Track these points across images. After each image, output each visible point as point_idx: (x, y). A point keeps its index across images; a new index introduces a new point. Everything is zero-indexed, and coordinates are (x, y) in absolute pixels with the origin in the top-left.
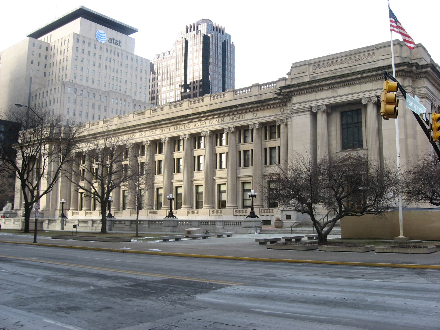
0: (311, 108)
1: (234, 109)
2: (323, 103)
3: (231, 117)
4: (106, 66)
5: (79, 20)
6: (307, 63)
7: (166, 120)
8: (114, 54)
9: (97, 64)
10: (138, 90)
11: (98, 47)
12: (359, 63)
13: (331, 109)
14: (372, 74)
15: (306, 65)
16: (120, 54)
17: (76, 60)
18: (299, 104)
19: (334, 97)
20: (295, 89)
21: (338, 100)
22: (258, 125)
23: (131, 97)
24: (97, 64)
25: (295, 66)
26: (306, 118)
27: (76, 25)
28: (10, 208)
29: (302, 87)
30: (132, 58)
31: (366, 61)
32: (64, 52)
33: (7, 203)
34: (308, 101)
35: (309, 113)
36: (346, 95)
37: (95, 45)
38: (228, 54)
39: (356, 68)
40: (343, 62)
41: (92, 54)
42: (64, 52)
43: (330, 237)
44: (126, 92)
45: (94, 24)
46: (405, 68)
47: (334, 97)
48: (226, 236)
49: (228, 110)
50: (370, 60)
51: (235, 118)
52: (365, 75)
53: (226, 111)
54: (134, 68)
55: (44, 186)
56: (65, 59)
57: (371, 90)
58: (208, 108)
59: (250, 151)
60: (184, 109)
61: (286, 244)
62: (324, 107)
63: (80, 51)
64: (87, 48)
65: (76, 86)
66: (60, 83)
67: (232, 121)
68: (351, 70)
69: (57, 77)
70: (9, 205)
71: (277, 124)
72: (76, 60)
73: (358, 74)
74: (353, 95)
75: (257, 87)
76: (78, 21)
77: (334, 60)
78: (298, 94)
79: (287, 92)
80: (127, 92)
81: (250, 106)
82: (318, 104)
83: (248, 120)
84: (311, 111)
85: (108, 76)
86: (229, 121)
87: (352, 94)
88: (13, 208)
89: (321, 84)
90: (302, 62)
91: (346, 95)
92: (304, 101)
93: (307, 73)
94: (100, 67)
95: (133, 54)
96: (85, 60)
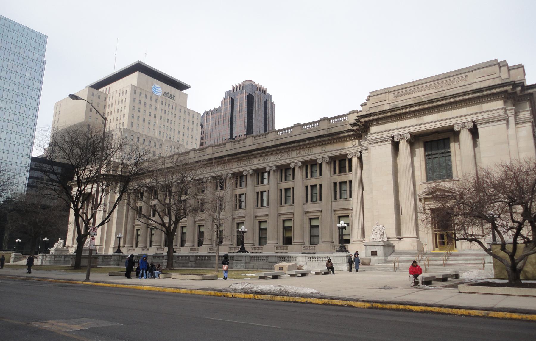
0: (393, 137)
1: (301, 143)
2: (407, 131)
3: (298, 152)
4: (161, 117)
5: (136, 74)
6: (387, 91)
7: (229, 155)
8: (169, 107)
9: (153, 115)
10: (190, 140)
11: (154, 100)
12: (449, 87)
13: (415, 139)
15: (385, 93)
16: (174, 107)
17: (133, 110)
18: (379, 134)
21: (425, 128)
22: (328, 159)
23: (184, 146)
24: (153, 115)
25: (372, 95)
26: (388, 148)
27: (134, 78)
28: (62, 245)
30: (185, 111)
31: (457, 86)
32: (122, 102)
33: (58, 240)
34: (389, 131)
35: (390, 142)
37: (151, 97)
38: (269, 111)
39: (445, 93)
40: (430, 87)
41: (148, 105)
42: (122, 102)
44: (178, 141)
45: (150, 78)
46: (509, 88)
47: (419, 125)
48: (300, 275)
49: (296, 144)
50: (463, 84)
51: (302, 153)
53: (293, 145)
54: (187, 120)
55: (99, 218)
56: (123, 109)
58: (273, 143)
59: (318, 186)
60: (247, 145)
62: (409, 136)
63: (137, 101)
64: (143, 98)
65: (133, 133)
66: (118, 129)
67: (299, 155)
68: (439, 95)
69: (115, 125)
70: (61, 241)
71: (349, 157)
72: (133, 110)
75: (326, 121)
76: (136, 74)
77: (418, 86)
79: (365, 122)
80: (180, 141)
81: (319, 140)
82: (401, 133)
83: (316, 154)
84: (393, 141)
85: (162, 126)
86: (295, 156)
88: (65, 244)
90: (380, 90)
93: (387, 102)
94: (155, 117)
95: (185, 108)
96: (142, 111)
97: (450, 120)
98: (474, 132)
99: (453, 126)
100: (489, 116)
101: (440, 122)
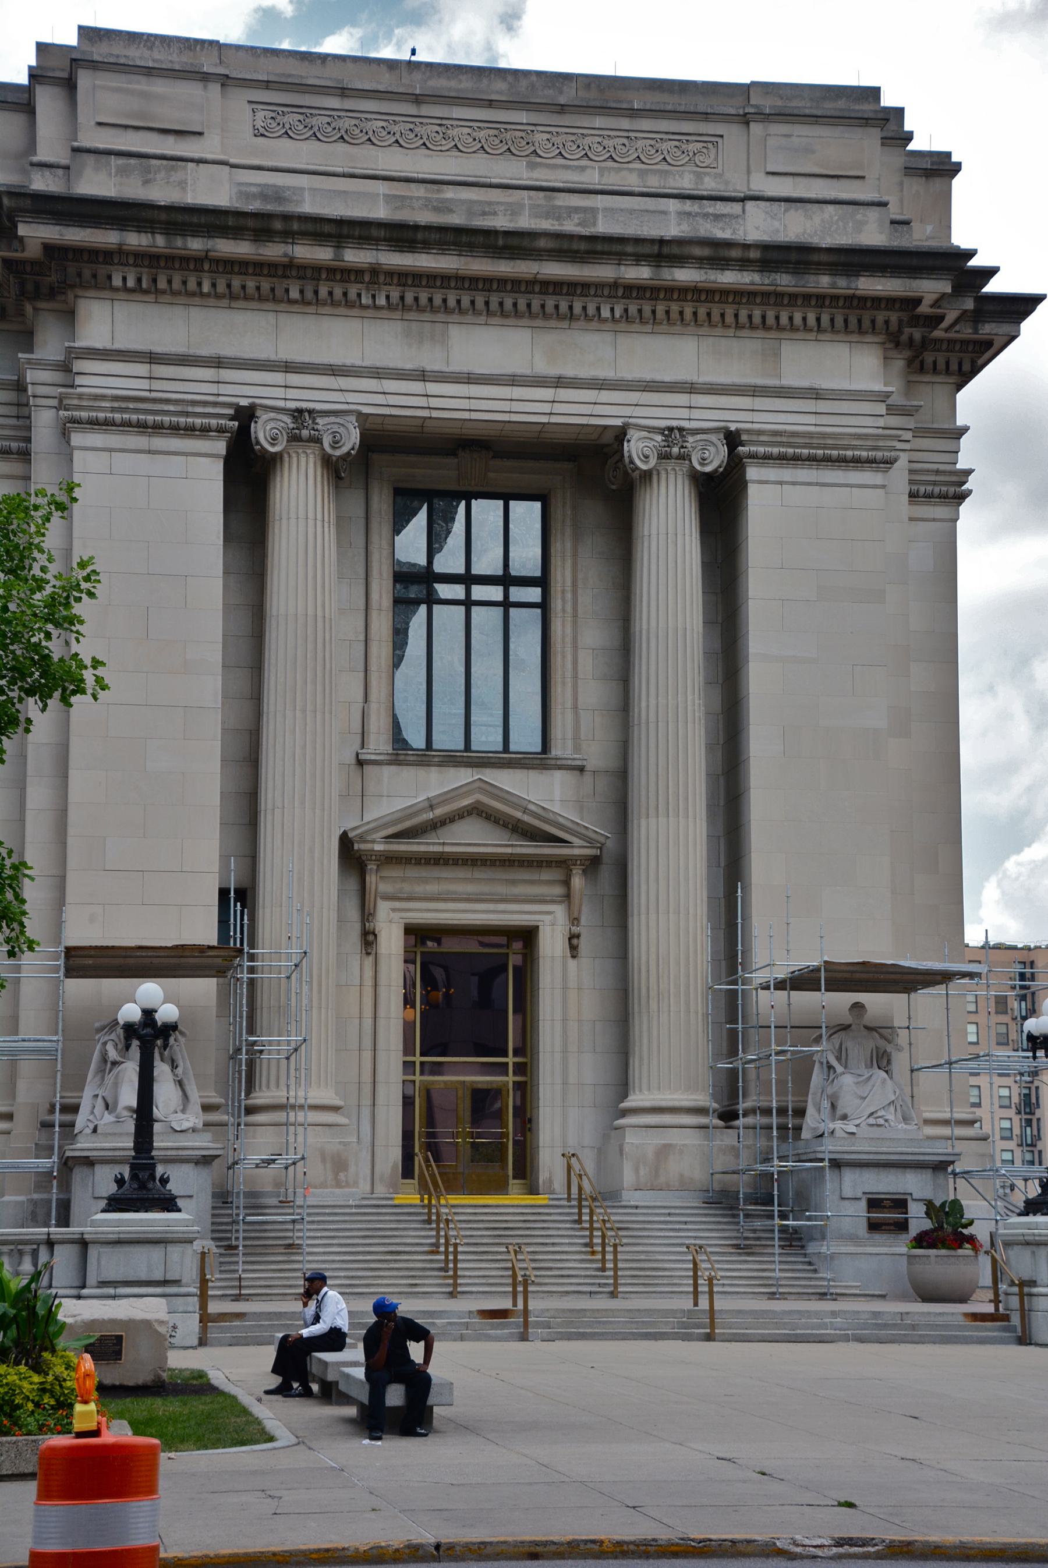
0: (246, 415)
14: (729, 278)
18: (142, 369)
19: (422, 376)
20: (135, 240)
29: (196, 245)
31: (654, 183)
34: (219, 362)
35: (221, 447)
36: (513, 381)
43: (53, 1402)
47: (422, 376)
52: (684, 275)
57: (691, 388)
61: (173, 1061)
62: (352, 439)
73: (639, 259)
74: (564, 394)
78: (138, 289)
87: (559, 382)
89: (355, 256)
91: (513, 381)
92: (181, 349)
97: (605, 396)
98: (720, 501)
99: (621, 434)
100: (137, 387)
101: (547, 393)
